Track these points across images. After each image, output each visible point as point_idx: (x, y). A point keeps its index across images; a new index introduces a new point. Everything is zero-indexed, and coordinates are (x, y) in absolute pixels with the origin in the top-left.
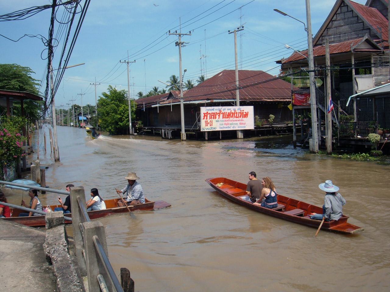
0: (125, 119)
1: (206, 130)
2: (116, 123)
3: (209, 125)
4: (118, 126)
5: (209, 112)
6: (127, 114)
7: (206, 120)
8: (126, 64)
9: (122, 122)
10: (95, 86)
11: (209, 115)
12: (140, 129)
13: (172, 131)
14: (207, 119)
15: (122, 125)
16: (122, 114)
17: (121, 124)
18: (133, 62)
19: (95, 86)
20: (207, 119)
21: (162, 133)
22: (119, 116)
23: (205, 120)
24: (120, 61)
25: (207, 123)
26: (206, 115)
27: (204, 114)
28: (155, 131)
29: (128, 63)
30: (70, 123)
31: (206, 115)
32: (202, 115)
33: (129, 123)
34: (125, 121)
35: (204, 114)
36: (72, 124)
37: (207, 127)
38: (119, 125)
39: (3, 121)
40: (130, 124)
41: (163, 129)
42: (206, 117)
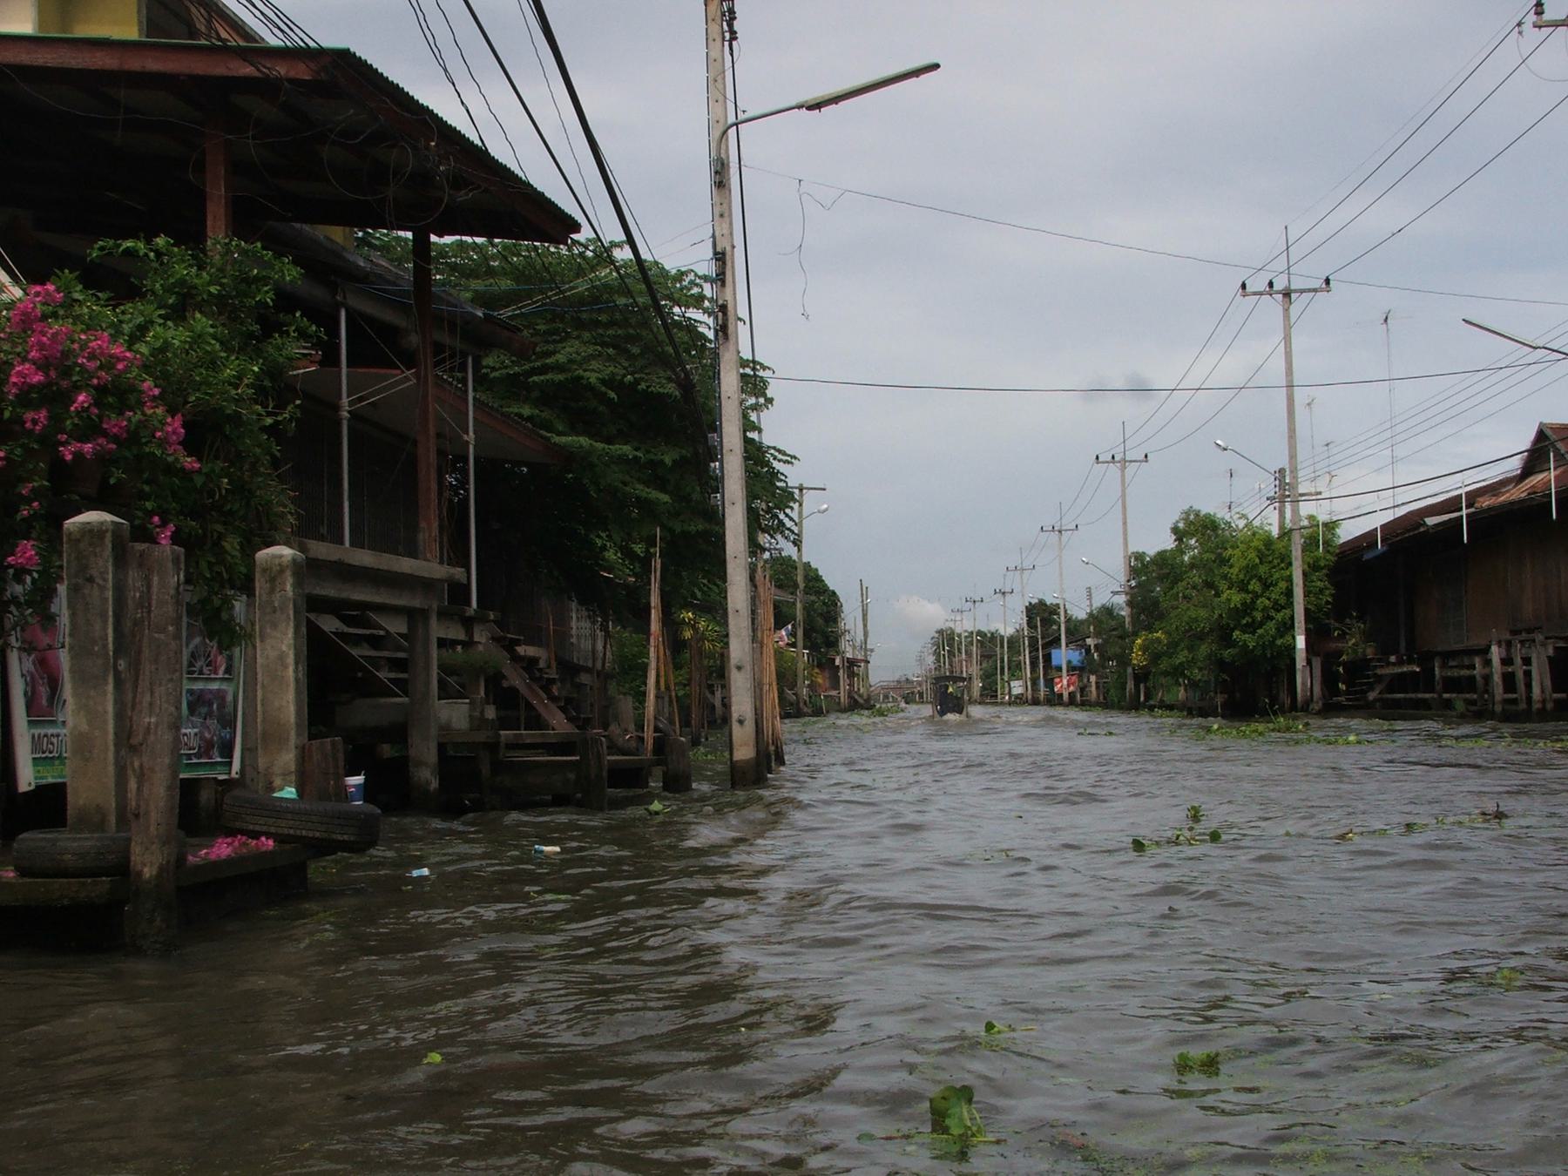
0: (1273, 613)
2: (1223, 634)
4: (1227, 654)
6: (1283, 585)
8: (1274, 305)
9: (1252, 628)
10: (1123, 469)
12: (1358, 669)
13: (1556, 649)
15: (1251, 645)
16: (1255, 586)
17: (1250, 640)
18: (1315, 290)
19: (1123, 469)
21: (1487, 678)
22: (1237, 598)
24: (1244, 286)
28: (1444, 666)
29: (1287, 294)
30: (1008, 682)
33: (1294, 638)
34: (1271, 625)
36: (1017, 688)
39: (1563, 1128)
40: (1301, 642)
41: (1499, 644)
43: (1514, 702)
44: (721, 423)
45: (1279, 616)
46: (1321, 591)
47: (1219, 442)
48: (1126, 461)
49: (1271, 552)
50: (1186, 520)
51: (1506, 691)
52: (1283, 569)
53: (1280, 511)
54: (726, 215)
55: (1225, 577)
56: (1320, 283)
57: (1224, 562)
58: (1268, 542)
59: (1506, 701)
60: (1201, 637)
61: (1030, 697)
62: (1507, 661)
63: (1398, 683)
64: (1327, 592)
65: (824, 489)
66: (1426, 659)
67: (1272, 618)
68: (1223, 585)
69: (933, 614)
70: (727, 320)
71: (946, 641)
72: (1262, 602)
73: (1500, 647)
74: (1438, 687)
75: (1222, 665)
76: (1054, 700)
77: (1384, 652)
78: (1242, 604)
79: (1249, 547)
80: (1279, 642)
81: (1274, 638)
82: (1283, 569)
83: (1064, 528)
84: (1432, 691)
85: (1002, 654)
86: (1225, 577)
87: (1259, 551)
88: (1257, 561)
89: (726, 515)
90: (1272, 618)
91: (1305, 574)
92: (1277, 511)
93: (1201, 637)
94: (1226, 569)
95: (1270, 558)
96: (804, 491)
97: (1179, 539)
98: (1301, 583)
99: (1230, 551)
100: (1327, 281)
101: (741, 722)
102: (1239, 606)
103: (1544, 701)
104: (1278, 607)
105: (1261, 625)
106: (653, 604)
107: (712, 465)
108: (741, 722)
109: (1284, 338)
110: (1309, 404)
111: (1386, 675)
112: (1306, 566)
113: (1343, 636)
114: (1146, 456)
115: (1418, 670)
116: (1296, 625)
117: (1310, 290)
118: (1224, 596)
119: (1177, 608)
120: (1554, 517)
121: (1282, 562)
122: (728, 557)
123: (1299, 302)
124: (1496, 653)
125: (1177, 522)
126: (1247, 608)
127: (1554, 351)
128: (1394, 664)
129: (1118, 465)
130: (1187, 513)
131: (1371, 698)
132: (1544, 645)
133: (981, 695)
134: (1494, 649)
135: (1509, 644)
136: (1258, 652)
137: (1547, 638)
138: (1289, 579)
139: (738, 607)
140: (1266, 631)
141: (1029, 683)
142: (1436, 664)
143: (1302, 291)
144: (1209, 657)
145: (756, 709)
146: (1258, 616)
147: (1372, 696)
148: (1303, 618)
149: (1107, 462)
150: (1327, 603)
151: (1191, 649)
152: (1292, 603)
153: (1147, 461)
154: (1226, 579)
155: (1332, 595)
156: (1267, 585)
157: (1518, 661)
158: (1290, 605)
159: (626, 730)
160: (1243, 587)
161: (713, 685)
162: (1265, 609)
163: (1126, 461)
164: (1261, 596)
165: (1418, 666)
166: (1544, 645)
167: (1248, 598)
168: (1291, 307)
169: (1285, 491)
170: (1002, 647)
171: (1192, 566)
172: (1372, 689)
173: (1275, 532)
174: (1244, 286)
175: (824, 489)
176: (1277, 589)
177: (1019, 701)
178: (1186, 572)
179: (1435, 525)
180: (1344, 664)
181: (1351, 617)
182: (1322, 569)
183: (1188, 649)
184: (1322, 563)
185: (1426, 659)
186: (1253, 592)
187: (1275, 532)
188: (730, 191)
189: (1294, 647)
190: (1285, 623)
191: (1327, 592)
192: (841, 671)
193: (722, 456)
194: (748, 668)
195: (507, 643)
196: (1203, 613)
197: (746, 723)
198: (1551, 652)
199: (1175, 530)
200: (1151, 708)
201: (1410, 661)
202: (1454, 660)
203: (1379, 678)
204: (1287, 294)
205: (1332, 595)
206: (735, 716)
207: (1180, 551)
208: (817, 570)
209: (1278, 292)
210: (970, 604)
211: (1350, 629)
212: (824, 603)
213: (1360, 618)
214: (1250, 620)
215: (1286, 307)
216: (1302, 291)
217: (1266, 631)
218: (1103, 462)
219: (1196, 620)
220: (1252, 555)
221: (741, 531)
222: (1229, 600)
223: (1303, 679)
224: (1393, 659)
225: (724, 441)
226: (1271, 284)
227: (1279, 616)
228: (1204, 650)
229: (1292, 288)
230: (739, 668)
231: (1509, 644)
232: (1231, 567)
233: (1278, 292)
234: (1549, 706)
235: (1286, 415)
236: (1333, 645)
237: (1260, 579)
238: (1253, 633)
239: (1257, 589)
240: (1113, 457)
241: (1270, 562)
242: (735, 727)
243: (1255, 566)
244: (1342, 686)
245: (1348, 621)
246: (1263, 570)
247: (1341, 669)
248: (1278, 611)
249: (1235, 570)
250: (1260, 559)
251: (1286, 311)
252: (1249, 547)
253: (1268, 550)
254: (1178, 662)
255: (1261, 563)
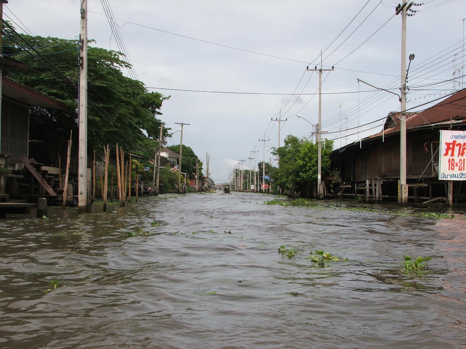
0: (312, 168)
1: (449, 179)
2: (297, 173)
3: (456, 168)
4: (298, 179)
5: (458, 141)
6: (315, 159)
7: (451, 158)
8: (317, 73)
9: (306, 172)
11: (457, 149)
12: (337, 185)
13: (383, 182)
14: (452, 155)
15: (305, 177)
16: (307, 159)
17: (305, 176)
20: (452, 155)
22: (301, 163)
23: (449, 156)
24: (308, 68)
25: (452, 164)
26: (450, 147)
27: (448, 144)
28: (357, 186)
29: (321, 71)
31: (451, 146)
32: (443, 148)
34: (311, 171)
35: (448, 144)
36: (252, 187)
37: (451, 172)
38: (299, 177)
40: (319, 177)
41: (369, 180)
42: (450, 152)
43: (372, 197)
44: (79, 96)
45: (314, 169)
46: (327, 162)
47: (298, 115)
48: (280, 120)
49: (312, 149)
50: (288, 138)
51: (370, 194)
52: (316, 154)
53: (316, 137)
54: (84, 28)
55: (298, 156)
56: (331, 68)
57: (299, 151)
58: (312, 146)
59: (370, 197)
60: (290, 174)
61: (256, 190)
62: (370, 185)
63: (347, 190)
64: (329, 162)
65: (189, 125)
66: (353, 184)
67: (311, 169)
68: (298, 159)
69: (233, 164)
70: (83, 62)
71: (237, 173)
72: (309, 164)
73: (369, 181)
74: (356, 192)
75: (296, 183)
76: (261, 191)
77: (343, 180)
78: (303, 165)
79: (306, 147)
80: (313, 177)
81: (312, 175)
82: (316, 154)
83: (265, 140)
84: (354, 194)
85: (249, 177)
86: (298, 156)
87: (309, 149)
88: (308, 152)
89: (80, 126)
90: (311, 169)
91: (322, 156)
92: (315, 137)
93: (290, 174)
94: (299, 154)
95: (312, 151)
96: (183, 125)
97: (286, 144)
98: (320, 159)
99: (300, 148)
100: (333, 68)
101: (81, 194)
102: (302, 165)
103: (379, 198)
104: (314, 166)
105: (308, 171)
106: (68, 155)
107: (76, 109)
108: (81, 194)
109: (321, 85)
110: (340, 106)
111: (344, 188)
112: (323, 154)
113: (333, 176)
114: (287, 119)
115: (351, 187)
116: (318, 172)
117: (327, 70)
118: (297, 162)
119: (283, 165)
120: (383, 141)
121: (316, 152)
122: (80, 140)
123: (324, 74)
124: (368, 182)
125: (285, 139)
126: (304, 166)
127: (390, 92)
128: (345, 185)
129: (278, 121)
130: (289, 136)
131: (338, 195)
132: (380, 181)
133: (243, 189)
134: (367, 181)
135: (371, 180)
136: (307, 179)
137: (381, 179)
138: (317, 158)
139: (82, 156)
140: (310, 173)
141: (255, 186)
142: (355, 185)
143: (325, 70)
144: (292, 180)
145: (87, 189)
146: (307, 168)
147: (339, 194)
148: (321, 170)
149: (275, 120)
150: (329, 165)
151: (287, 177)
152: (318, 165)
153: (287, 121)
154: (299, 157)
155: (331, 163)
156: (311, 159)
157: (373, 185)
158: (317, 165)
159: (69, 195)
160: (303, 159)
161: (141, 182)
162: (310, 166)
163: (280, 120)
164: (309, 162)
165: (351, 185)
166: (380, 181)
167: (305, 163)
168: (322, 75)
169: (318, 132)
170: (249, 175)
171: (289, 152)
172: (339, 192)
173: (314, 143)
174: (308, 68)
175: (189, 125)
176: (314, 161)
177: (253, 191)
178: (287, 154)
179: (357, 143)
180: (333, 184)
181: (335, 170)
182: (328, 155)
183: (286, 177)
184: (328, 153)
185: (353, 184)
186: (306, 161)
187: (314, 143)
188: (87, 20)
189: (318, 178)
190: (316, 171)
191: (329, 162)
192: (197, 180)
193: (79, 107)
194: (84, 176)
195: (35, 165)
196: (291, 167)
197: (83, 194)
198: (382, 183)
199: (285, 141)
200: (283, 195)
201: (349, 184)
202: (360, 184)
203: (341, 189)
204: (321, 71)
205: (331, 163)
206: (79, 192)
207: (285, 148)
208: (192, 149)
209: (318, 70)
210: (241, 162)
211: (335, 174)
212: (194, 159)
213: (338, 170)
214: (305, 170)
215: (320, 75)
216: (325, 70)
217: (310, 173)
218: (273, 120)
219: (288, 169)
220: (307, 150)
221: (84, 131)
222: (299, 163)
223: (320, 188)
224: (344, 183)
225: (80, 101)
226: (316, 68)
227: (314, 169)
228: (290, 178)
229: (322, 69)
230: (81, 176)
231: (371, 180)
232: (300, 153)
233: (318, 70)
234: (381, 199)
235: (318, 107)
236: (329, 178)
237: (309, 157)
238: (306, 173)
239: (307, 160)
240: (277, 119)
241: (312, 152)
242: (79, 194)
243: (307, 153)
244: (332, 191)
245: (334, 171)
246: (309, 154)
247: (332, 186)
248: (314, 167)
249: (301, 154)
250: (309, 151)
251: (320, 76)
252: (306, 147)
253: (312, 148)
254: (282, 181)
255: (309, 152)
